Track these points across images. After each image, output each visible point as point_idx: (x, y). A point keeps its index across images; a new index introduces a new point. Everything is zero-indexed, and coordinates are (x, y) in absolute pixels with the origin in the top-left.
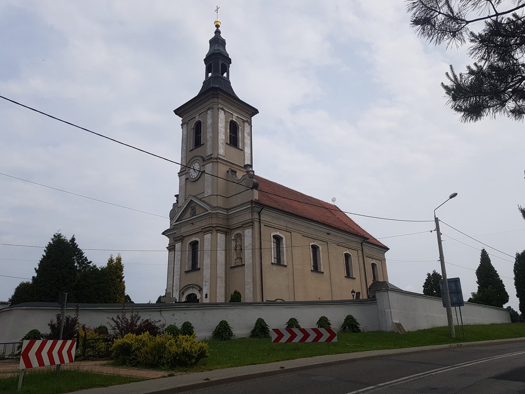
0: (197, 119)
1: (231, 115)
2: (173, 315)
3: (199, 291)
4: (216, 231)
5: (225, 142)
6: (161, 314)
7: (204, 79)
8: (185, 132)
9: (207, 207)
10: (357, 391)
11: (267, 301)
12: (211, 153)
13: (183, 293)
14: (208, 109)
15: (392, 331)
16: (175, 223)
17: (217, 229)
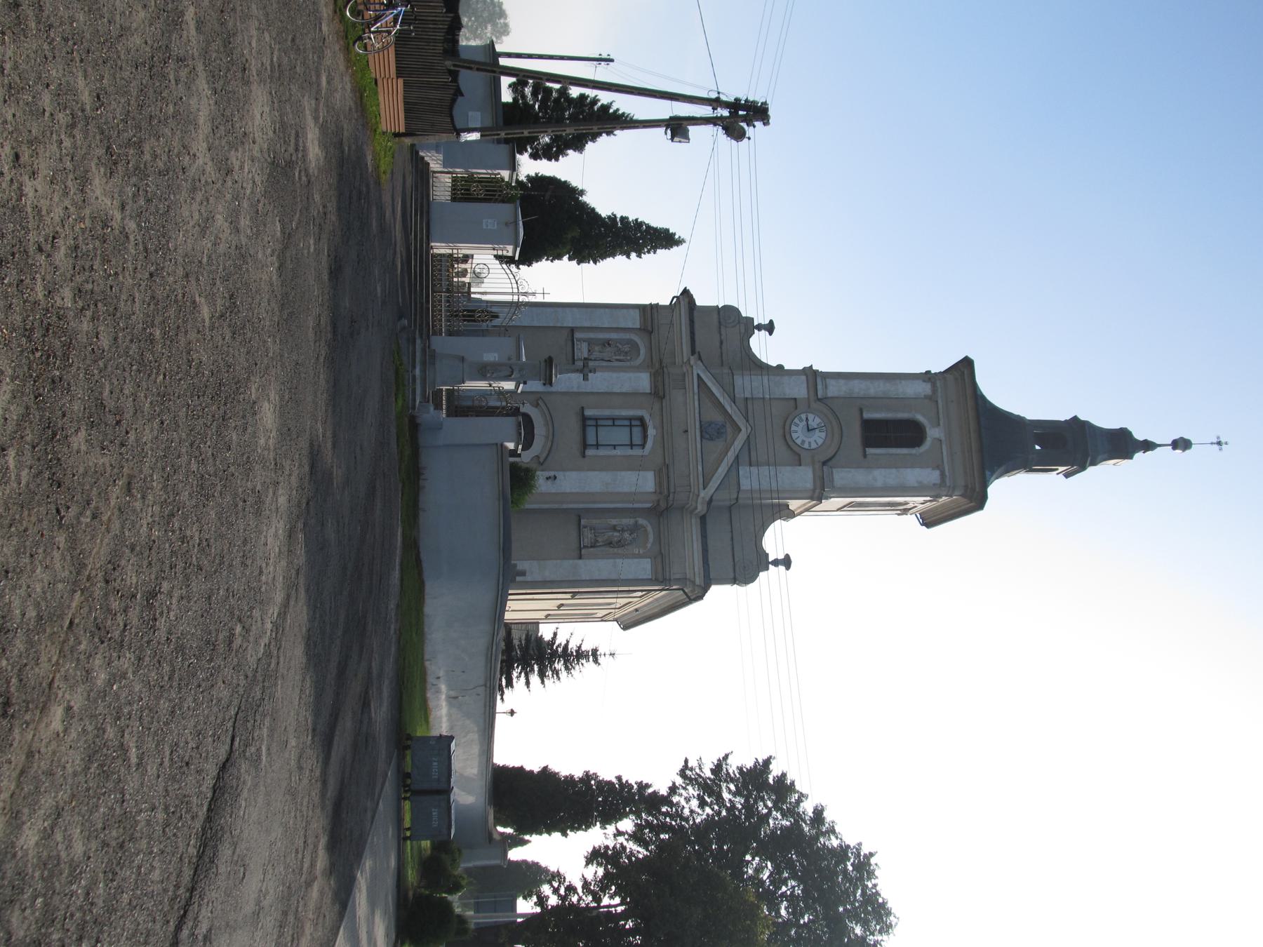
0: (933, 433)
4: (659, 501)
13: (537, 405)
14: (943, 475)
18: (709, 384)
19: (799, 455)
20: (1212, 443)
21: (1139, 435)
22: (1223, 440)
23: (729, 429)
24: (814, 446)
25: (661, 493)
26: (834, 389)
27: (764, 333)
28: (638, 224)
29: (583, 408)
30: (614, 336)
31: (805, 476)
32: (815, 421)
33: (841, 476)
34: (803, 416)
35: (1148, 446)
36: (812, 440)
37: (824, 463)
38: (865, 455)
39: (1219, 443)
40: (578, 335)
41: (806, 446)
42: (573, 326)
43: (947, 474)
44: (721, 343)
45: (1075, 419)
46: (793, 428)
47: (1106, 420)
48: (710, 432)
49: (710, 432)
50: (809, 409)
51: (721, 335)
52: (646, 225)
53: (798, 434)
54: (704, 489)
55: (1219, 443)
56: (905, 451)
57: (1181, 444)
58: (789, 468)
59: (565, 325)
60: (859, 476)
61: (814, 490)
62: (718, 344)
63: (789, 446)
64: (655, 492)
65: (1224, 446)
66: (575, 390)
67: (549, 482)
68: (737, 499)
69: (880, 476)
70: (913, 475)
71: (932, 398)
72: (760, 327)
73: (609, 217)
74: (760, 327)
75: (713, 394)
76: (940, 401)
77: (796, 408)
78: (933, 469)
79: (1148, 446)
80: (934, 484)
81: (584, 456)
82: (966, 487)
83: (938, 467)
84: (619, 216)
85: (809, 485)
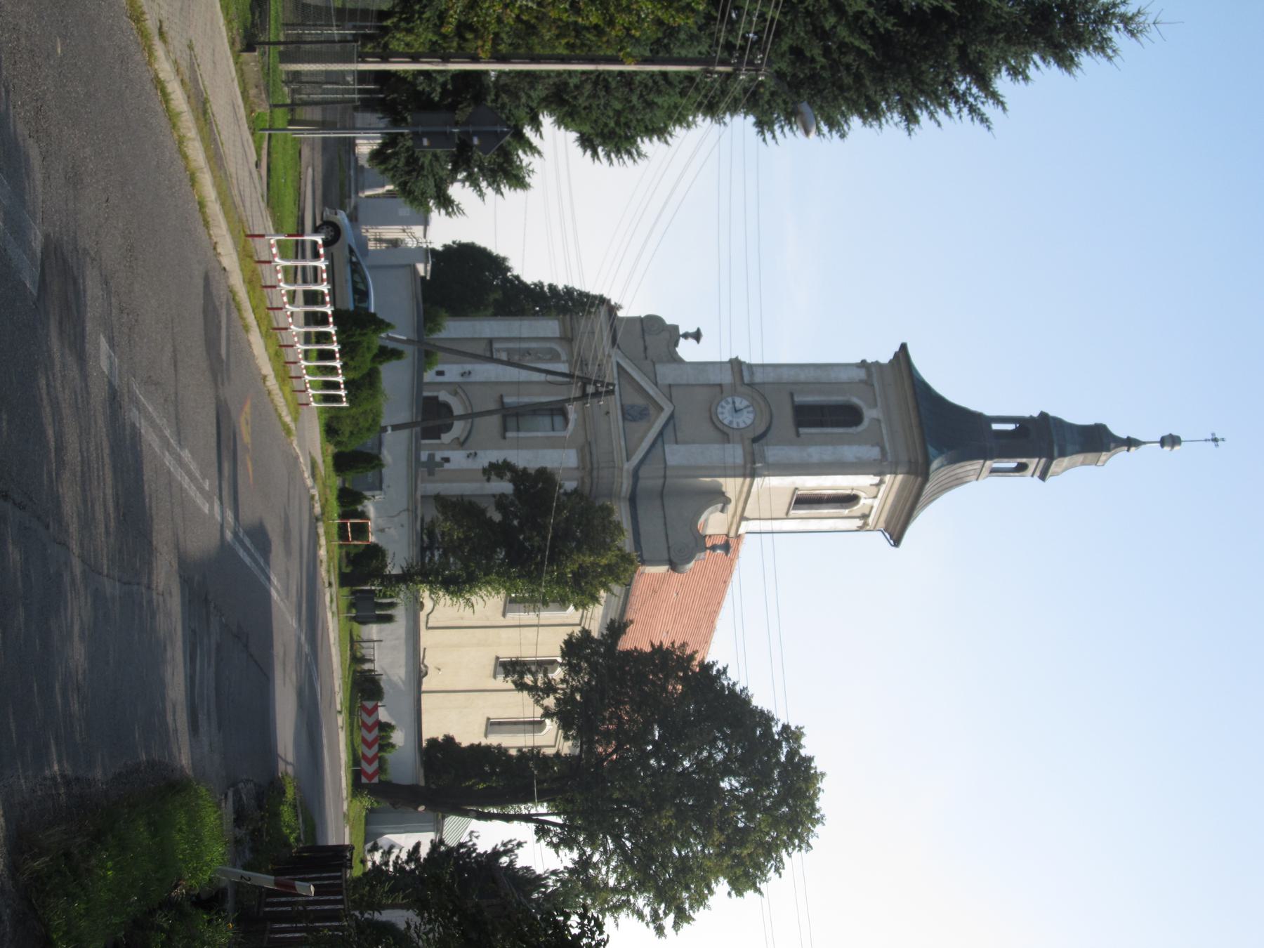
0: (870, 414)
1: (874, 494)
2: (402, 526)
3: (458, 438)
4: (582, 478)
5: (732, 560)
6: (399, 514)
7: (989, 412)
8: (844, 376)
9: (636, 459)
10: (53, 461)
11: (425, 649)
12: (771, 459)
13: (455, 394)
14: (883, 450)
15: (416, 203)
16: (619, 365)
17: (586, 480)
18: (629, 370)
19: (728, 435)
20: (1206, 440)
21: (1119, 431)
22: (1218, 436)
23: (652, 411)
24: (742, 425)
25: (584, 468)
26: (758, 378)
27: (692, 341)
28: (569, 291)
29: (501, 397)
30: (533, 345)
31: (735, 453)
32: (741, 403)
33: (774, 453)
34: (730, 400)
35: (1130, 443)
36: (740, 420)
37: (755, 440)
38: (798, 435)
39: (1215, 440)
40: (496, 345)
41: (735, 426)
42: (492, 336)
43: (889, 451)
44: (645, 348)
45: (1043, 416)
46: (720, 410)
47: (1077, 414)
48: (631, 415)
49: (631, 415)
50: (734, 392)
51: (644, 341)
52: (576, 291)
53: (725, 415)
54: (628, 460)
55: (1215, 440)
56: (841, 430)
57: (1170, 441)
58: (717, 446)
59: (483, 336)
60: (793, 453)
61: (745, 466)
62: (642, 349)
63: (713, 423)
64: (577, 468)
65: (1220, 443)
66: (493, 379)
67: (470, 460)
68: (665, 477)
69: (815, 453)
70: (850, 452)
71: (868, 383)
72: (686, 336)
73: (535, 285)
74: (686, 336)
75: (633, 379)
76: (876, 385)
77: (722, 392)
78: (873, 446)
79: (1130, 443)
80: (875, 460)
81: (504, 438)
82: (910, 462)
83: (877, 444)
84: (546, 284)
85: (739, 460)
